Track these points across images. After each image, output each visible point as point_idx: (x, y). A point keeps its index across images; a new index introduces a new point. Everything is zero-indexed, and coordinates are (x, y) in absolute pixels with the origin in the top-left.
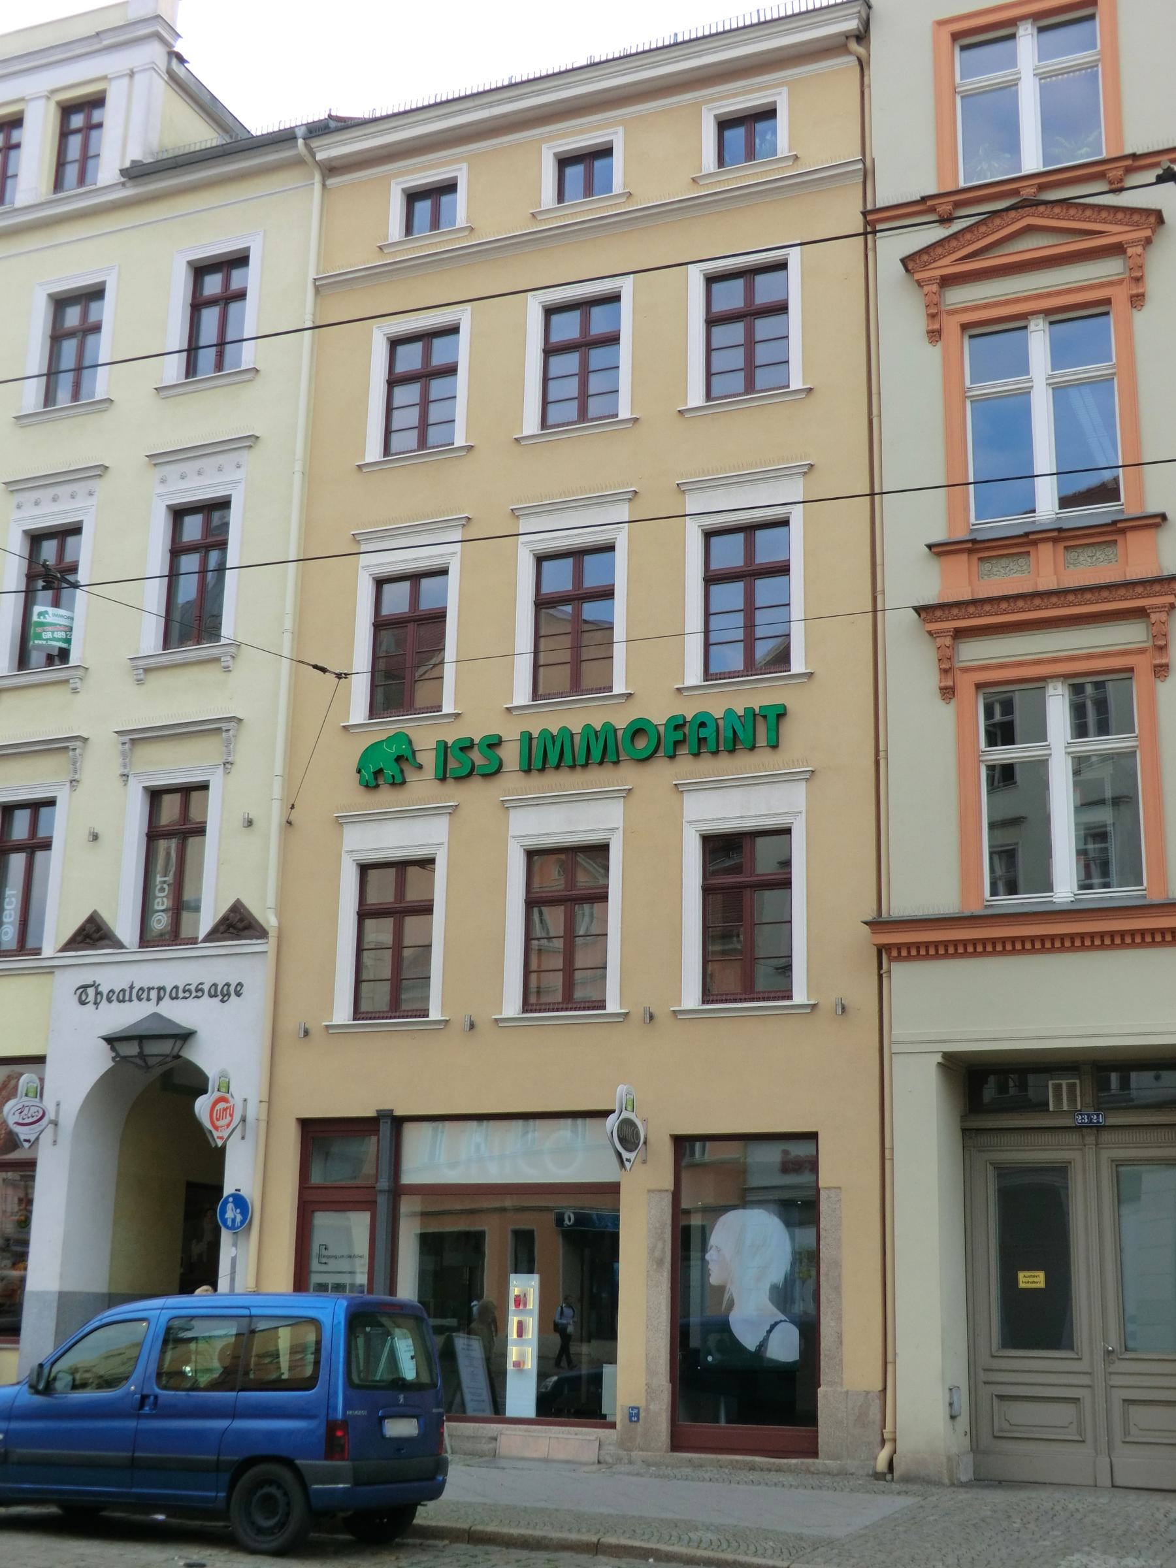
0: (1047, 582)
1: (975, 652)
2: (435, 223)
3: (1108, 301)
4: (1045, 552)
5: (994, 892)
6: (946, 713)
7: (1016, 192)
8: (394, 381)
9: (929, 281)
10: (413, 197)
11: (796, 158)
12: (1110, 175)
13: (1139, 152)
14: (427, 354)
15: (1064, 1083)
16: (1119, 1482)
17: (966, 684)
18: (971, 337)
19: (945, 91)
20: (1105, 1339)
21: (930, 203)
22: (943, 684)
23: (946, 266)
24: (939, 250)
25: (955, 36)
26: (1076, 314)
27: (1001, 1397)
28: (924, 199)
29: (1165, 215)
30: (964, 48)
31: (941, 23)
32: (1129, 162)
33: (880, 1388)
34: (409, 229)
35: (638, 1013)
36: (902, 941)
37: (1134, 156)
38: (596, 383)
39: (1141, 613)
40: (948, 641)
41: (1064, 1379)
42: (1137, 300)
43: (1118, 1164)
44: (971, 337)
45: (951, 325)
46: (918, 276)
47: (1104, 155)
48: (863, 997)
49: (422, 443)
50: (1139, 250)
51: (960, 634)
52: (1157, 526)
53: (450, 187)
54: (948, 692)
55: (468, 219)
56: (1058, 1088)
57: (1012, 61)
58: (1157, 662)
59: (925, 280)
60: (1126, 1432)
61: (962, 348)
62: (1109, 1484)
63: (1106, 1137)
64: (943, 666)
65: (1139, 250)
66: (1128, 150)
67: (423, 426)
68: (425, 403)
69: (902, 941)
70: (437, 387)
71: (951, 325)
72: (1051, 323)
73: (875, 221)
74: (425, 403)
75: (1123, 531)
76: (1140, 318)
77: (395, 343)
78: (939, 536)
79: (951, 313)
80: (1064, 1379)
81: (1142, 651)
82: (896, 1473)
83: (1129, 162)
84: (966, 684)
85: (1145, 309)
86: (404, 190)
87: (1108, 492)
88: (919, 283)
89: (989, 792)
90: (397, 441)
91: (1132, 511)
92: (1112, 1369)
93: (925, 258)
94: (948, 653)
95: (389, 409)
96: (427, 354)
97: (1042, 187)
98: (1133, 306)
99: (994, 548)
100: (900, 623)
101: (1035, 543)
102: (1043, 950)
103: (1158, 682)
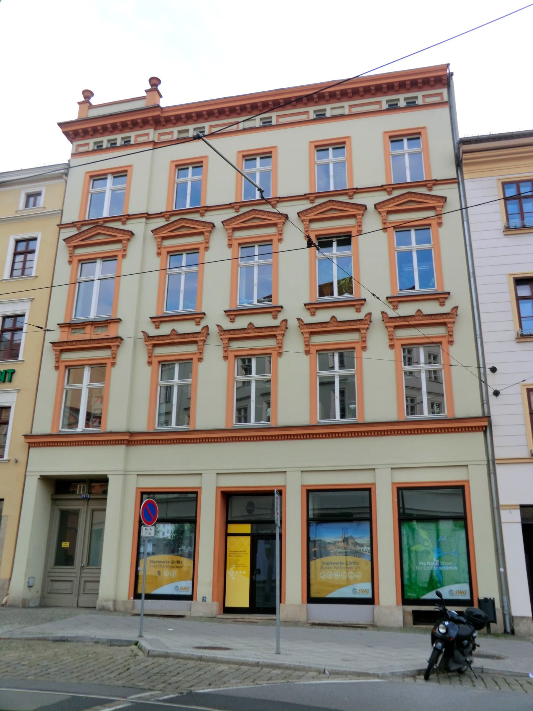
0: (87, 337)
2: (34, 205)
4: (88, 328)
5: (408, 414)
6: (224, 364)
7: (97, 222)
8: (16, 254)
9: (383, 212)
10: (29, 196)
11: (44, 208)
12: (201, 212)
13: (438, 179)
14: (27, 246)
15: (82, 485)
16: (80, 605)
18: (242, 248)
19: (171, 181)
20: (82, 562)
21: (384, 187)
22: (391, 344)
24: (74, 238)
26: (423, 227)
27: (52, 581)
29: (289, 216)
32: (355, 190)
33: (9, 577)
34: (27, 206)
35: (13, 459)
36: (35, 441)
37: (357, 189)
38: (28, 265)
41: (61, 575)
43: (93, 511)
44: (242, 248)
45: (164, 252)
46: (302, 218)
47: (347, 188)
48: (22, 459)
49: (23, 274)
50: (208, 234)
52: (118, 322)
53: (39, 194)
54: (392, 346)
55: (44, 205)
56: (80, 487)
57: (105, 185)
58: (363, 346)
59: (382, 211)
60: (84, 590)
62: (76, 606)
63: (90, 502)
64: (306, 344)
65: (281, 225)
66: (278, 196)
67: (24, 268)
68: (25, 261)
69: (35, 441)
70: (29, 256)
72: (104, 261)
73: (61, 226)
74: (25, 261)
75: (109, 323)
76: (441, 230)
77: (17, 242)
78: (227, 308)
79: (76, 256)
80: (61, 575)
82: (7, 604)
83: (355, 190)
85: (209, 251)
86: (26, 193)
87: (269, 298)
88: (302, 221)
89: (355, 382)
90: (15, 273)
92: (83, 571)
93: (70, 240)
95: (14, 262)
96: (27, 246)
97: (105, 222)
98: (123, 258)
99: (99, 324)
100: (48, 346)
101: (86, 325)
103: (363, 352)
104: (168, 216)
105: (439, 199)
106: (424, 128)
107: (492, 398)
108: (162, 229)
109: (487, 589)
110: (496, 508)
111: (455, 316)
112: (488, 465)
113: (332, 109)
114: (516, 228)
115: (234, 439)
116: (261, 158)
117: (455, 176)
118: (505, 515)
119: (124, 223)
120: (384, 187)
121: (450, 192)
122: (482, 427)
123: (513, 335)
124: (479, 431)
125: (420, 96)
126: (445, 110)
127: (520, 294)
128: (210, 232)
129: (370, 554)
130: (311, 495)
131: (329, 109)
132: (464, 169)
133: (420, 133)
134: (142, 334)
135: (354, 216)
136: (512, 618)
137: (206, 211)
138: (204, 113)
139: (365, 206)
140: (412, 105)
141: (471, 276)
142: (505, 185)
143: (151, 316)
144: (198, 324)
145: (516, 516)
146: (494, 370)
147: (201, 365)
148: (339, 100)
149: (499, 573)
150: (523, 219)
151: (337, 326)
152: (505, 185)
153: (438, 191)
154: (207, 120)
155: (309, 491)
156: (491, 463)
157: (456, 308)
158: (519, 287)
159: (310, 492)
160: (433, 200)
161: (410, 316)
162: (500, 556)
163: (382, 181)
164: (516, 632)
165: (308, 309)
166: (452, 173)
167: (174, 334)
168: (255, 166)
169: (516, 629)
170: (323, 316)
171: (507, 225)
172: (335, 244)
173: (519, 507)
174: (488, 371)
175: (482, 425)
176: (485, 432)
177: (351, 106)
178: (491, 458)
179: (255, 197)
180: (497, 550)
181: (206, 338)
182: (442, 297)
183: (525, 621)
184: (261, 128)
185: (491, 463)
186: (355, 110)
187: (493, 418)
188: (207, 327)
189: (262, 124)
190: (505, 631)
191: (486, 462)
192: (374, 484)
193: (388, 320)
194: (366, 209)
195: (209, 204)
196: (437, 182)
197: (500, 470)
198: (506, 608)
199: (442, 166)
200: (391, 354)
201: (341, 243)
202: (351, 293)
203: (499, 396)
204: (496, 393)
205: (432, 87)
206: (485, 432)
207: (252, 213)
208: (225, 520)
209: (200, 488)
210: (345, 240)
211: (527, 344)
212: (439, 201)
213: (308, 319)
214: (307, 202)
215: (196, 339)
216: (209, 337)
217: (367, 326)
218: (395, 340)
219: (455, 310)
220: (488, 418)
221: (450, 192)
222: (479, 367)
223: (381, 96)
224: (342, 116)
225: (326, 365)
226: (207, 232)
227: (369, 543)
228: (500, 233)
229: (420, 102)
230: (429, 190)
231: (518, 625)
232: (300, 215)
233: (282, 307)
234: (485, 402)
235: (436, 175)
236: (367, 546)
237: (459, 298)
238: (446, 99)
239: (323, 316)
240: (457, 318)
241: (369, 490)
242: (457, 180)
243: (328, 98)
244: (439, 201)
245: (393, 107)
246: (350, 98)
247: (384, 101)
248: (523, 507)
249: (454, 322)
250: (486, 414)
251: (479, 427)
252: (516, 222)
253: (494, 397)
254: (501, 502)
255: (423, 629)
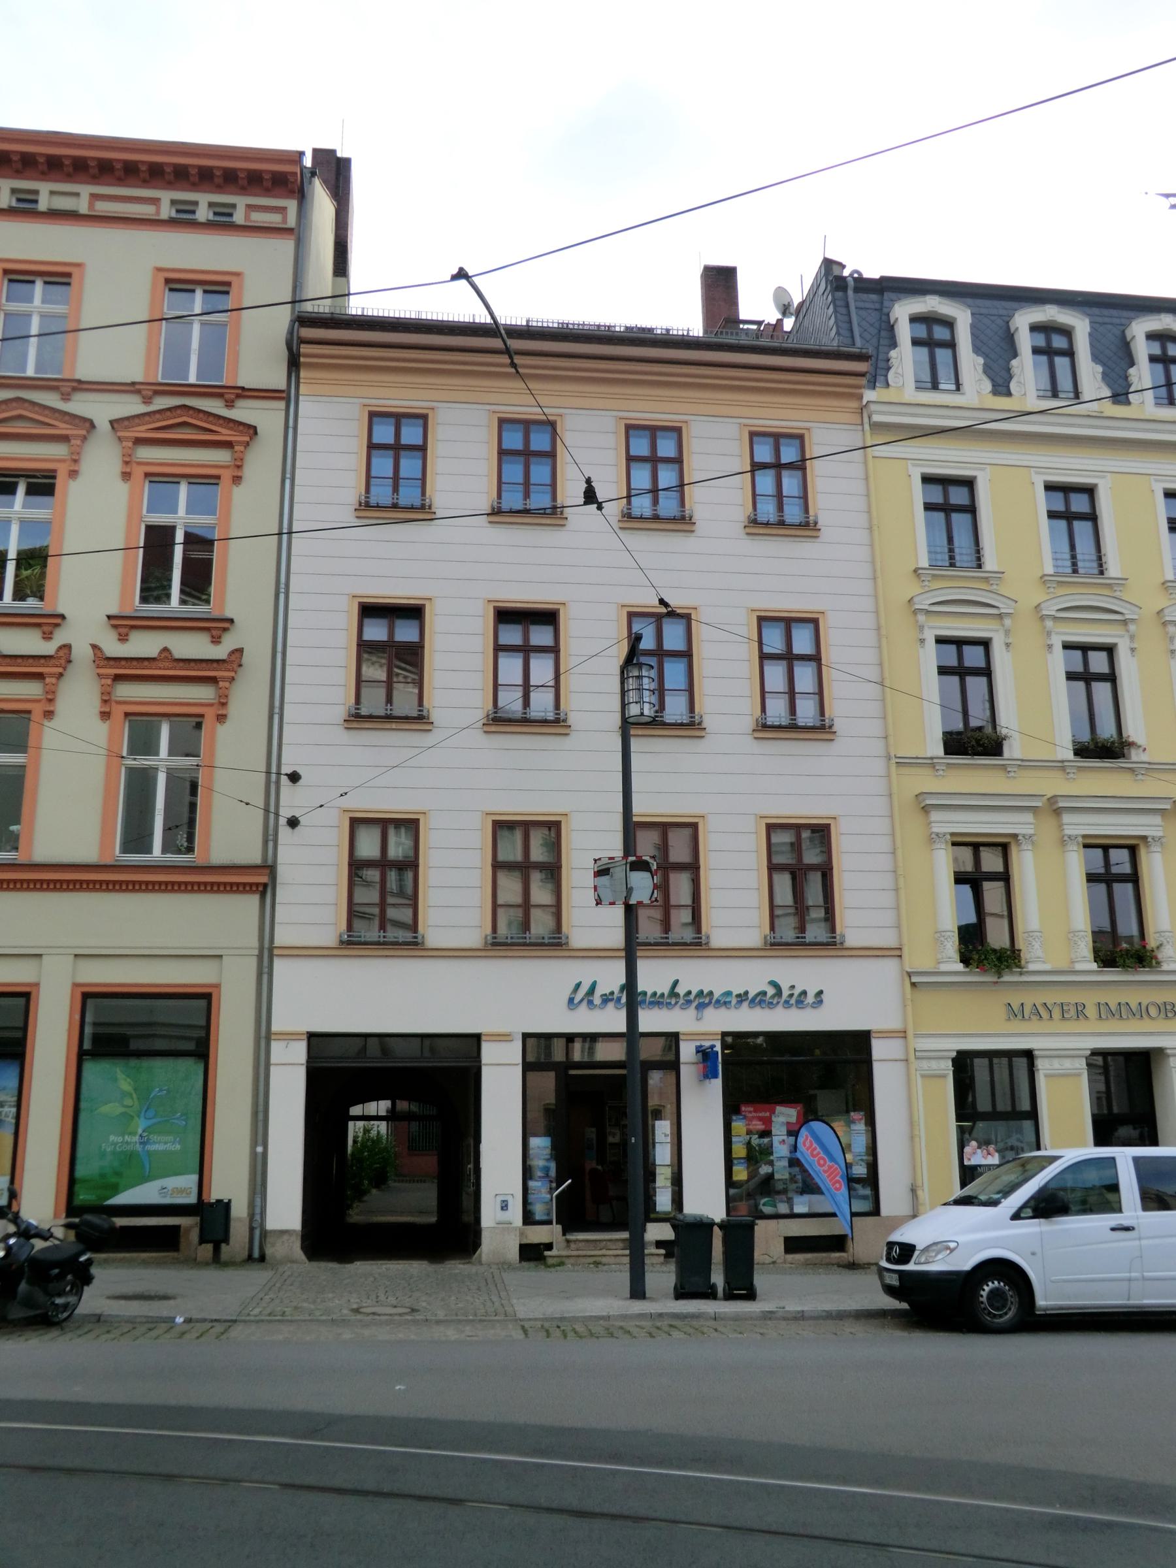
1: (126, 691)
3: (218, 477)
9: (127, 438)
12: (227, 396)
13: (247, 386)
17: (118, 712)
21: (138, 387)
23: (141, 431)
25: (168, 281)
28: (133, 384)
30: (171, 290)
31: (159, 270)
32: (75, 384)
37: (79, 381)
39: (40, 676)
40: (109, 682)
42: (237, 480)
45: (138, 472)
46: (120, 434)
50: (79, 442)
51: (118, 678)
54: (105, 715)
61: (143, 490)
66: (77, 377)
71: (138, 472)
76: (238, 492)
78: (114, 611)
81: (211, 705)
83: (75, 384)
84: (118, 712)
91: (216, 614)
93: (126, 423)
94: (108, 689)
102: (192, 891)
104: (150, 393)
105: (241, 428)
106: (78, 265)
107: (284, 832)
108: (137, 421)
109: (228, 1183)
110: (264, 1037)
111: (235, 666)
112: (260, 957)
113: (52, 193)
114: (767, 524)
115: (137, 887)
116: (205, 292)
117: (282, 385)
118: (278, 1050)
119: (66, 398)
120: (138, 387)
121: (266, 418)
122: (257, 885)
123: (341, 713)
124: (251, 891)
125: (241, 205)
126: (287, 246)
127: (503, 641)
128: (84, 438)
129: (13, 1121)
130: (90, 1003)
131: (47, 193)
132: (303, 374)
133: (229, 284)
134: (90, 651)
135: (228, 445)
136: (265, 1234)
137: (238, 396)
138: (92, 164)
139: (255, 428)
140: (222, 222)
141: (281, 590)
142: (374, 416)
143: (109, 613)
144: (48, 637)
145: (299, 1052)
146: (294, 777)
147: (223, 731)
148: (69, 178)
149: (254, 1154)
150: (396, 489)
151: (171, 669)
152: (374, 416)
153: (244, 412)
154: (243, 191)
155: (86, 996)
156: (267, 954)
157: (240, 651)
158: (502, 628)
159: (88, 997)
160: (231, 429)
161: (217, 661)
162: (260, 1124)
163: (136, 373)
164: (267, 1257)
165: (115, 627)
166: (277, 378)
167: (166, 658)
168: (30, 299)
169: (269, 1251)
170: (144, 645)
171: (626, 511)
172: (21, 490)
173: (305, 1037)
174: (284, 779)
175: (259, 880)
176: (263, 895)
177: (94, 197)
178: (266, 945)
179: (24, 371)
180: (255, 1114)
181: (65, 669)
182: (219, 627)
183: (286, 1237)
184: (172, 223)
185: (267, 954)
186: (103, 207)
187: (280, 870)
188: (67, 647)
189: (211, 217)
190: (250, 1258)
191: (256, 952)
192: (217, 986)
193: (102, 663)
194: (256, 433)
195: (80, 375)
196: (244, 393)
197: (280, 967)
198: (258, 1217)
199: (258, 358)
200: (99, 731)
201: (32, 491)
202: (42, 598)
203: (298, 828)
204: (293, 823)
205: (267, 192)
206: (263, 895)
207: (14, 404)
208: (75, 1049)
209: (37, 985)
210: (42, 486)
211: (364, 733)
212: (242, 433)
213: (113, 648)
214: (136, 399)
215: (45, 670)
216: (70, 667)
217: (60, 670)
218: (113, 704)
219: (237, 655)
220: (270, 868)
221: (266, 418)
222: (268, 773)
223: (81, 183)
224: (71, 216)
225: (143, 743)
226: (76, 436)
227: (15, 1099)
228: (738, 529)
229: (239, 217)
230: (144, 403)
231: (273, 1245)
232: (116, 425)
233: (63, 617)
234: (270, 838)
235: (246, 379)
236: (10, 1106)
237: (251, 635)
238: (292, 222)
239: (144, 645)
240: (240, 670)
241: (26, 996)
242: (284, 395)
243: (269, 184)
244: (241, 432)
245: (184, 220)
246: (95, 179)
247: (166, 200)
248: (312, 1037)
249: (233, 679)
250: (270, 862)
251: (251, 885)
252: (513, 500)
253: (288, 829)
254: (275, 1028)
255: (121, 1260)
